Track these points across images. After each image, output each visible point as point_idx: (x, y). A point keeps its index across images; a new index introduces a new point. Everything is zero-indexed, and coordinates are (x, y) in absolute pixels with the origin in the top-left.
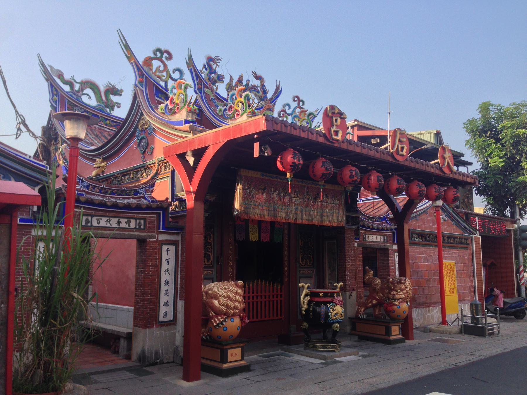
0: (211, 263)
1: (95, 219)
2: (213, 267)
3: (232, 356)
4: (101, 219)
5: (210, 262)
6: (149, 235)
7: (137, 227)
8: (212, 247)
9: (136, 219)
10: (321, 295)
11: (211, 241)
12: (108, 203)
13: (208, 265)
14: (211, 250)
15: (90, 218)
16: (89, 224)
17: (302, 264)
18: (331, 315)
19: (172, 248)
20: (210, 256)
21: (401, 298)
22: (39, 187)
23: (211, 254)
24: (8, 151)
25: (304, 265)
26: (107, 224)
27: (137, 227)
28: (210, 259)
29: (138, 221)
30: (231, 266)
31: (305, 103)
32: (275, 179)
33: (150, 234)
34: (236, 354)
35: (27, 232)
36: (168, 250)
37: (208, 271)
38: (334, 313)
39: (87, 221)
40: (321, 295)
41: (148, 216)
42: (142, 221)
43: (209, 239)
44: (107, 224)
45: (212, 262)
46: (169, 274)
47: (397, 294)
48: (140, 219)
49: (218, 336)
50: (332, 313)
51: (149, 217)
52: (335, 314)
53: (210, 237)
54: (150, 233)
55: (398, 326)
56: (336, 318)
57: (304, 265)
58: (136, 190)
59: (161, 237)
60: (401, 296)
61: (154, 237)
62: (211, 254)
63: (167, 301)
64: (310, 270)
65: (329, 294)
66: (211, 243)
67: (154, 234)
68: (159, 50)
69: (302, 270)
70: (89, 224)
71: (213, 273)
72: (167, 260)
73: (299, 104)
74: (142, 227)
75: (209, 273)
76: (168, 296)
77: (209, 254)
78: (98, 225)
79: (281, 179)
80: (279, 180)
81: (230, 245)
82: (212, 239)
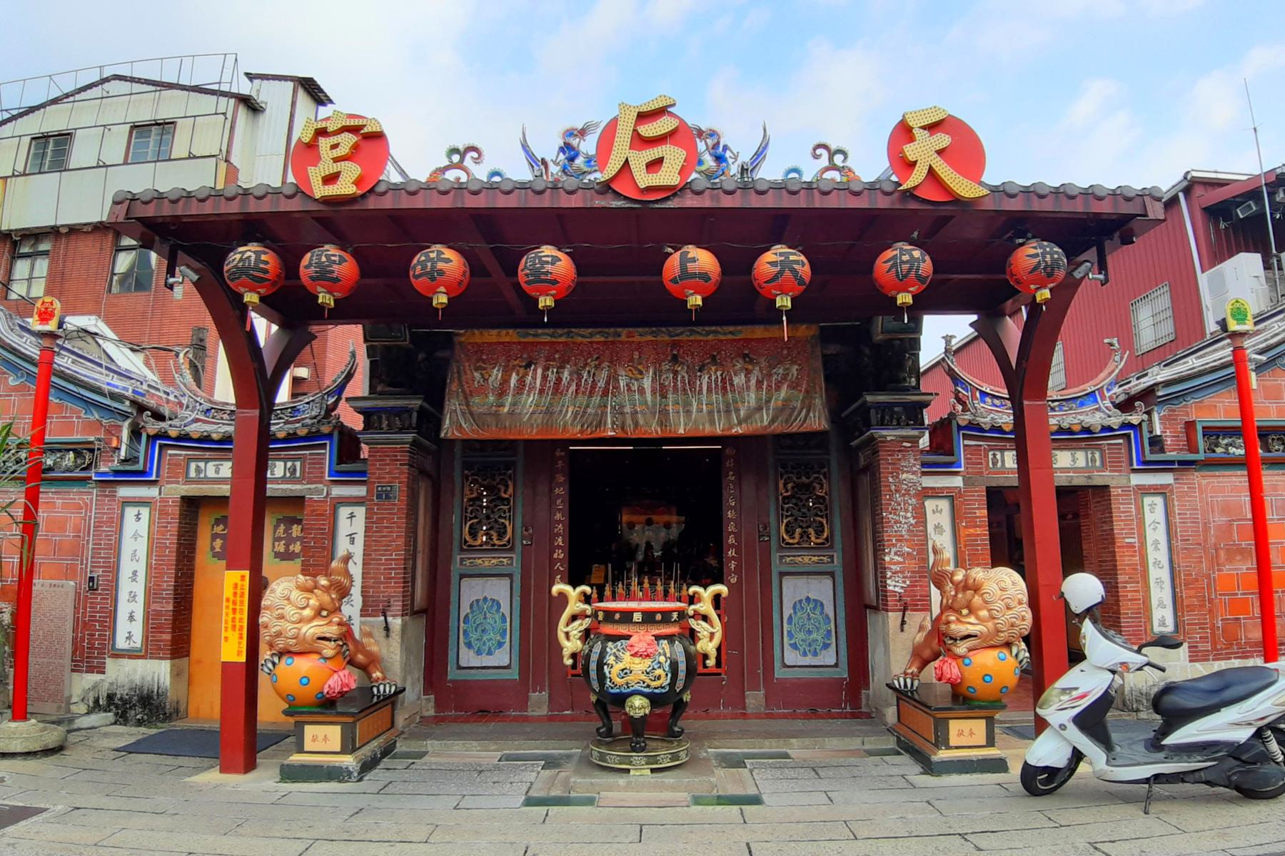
0: (509, 541)
1: (211, 465)
2: (512, 549)
3: (314, 739)
4: (221, 465)
5: (506, 539)
6: (310, 489)
7: (288, 475)
9: (285, 460)
11: (507, 496)
12: (215, 436)
14: (507, 514)
15: (202, 464)
17: (791, 541)
18: (610, 673)
19: (360, 512)
20: (505, 527)
22: (129, 421)
24: (85, 376)
25: (797, 543)
28: (505, 532)
29: (289, 464)
30: (732, 546)
31: (850, 156)
35: (112, 492)
36: (352, 516)
37: (499, 558)
39: (198, 470)
41: (308, 452)
42: (298, 464)
43: (503, 490)
45: (509, 539)
46: (355, 564)
48: (294, 459)
49: (288, 695)
50: (612, 667)
52: (623, 670)
53: (507, 487)
54: (312, 484)
55: (463, 664)
56: (627, 683)
57: (797, 543)
58: (295, 407)
59: (338, 491)
61: (319, 492)
62: (825, 522)
63: (350, 617)
64: (819, 556)
65: (617, 616)
66: (508, 500)
67: (320, 486)
68: (454, 151)
69: (470, 559)
70: (202, 475)
71: (512, 564)
72: (351, 535)
73: (831, 159)
74: (298, 474)
76: (352, 605)
82: (511, 490)
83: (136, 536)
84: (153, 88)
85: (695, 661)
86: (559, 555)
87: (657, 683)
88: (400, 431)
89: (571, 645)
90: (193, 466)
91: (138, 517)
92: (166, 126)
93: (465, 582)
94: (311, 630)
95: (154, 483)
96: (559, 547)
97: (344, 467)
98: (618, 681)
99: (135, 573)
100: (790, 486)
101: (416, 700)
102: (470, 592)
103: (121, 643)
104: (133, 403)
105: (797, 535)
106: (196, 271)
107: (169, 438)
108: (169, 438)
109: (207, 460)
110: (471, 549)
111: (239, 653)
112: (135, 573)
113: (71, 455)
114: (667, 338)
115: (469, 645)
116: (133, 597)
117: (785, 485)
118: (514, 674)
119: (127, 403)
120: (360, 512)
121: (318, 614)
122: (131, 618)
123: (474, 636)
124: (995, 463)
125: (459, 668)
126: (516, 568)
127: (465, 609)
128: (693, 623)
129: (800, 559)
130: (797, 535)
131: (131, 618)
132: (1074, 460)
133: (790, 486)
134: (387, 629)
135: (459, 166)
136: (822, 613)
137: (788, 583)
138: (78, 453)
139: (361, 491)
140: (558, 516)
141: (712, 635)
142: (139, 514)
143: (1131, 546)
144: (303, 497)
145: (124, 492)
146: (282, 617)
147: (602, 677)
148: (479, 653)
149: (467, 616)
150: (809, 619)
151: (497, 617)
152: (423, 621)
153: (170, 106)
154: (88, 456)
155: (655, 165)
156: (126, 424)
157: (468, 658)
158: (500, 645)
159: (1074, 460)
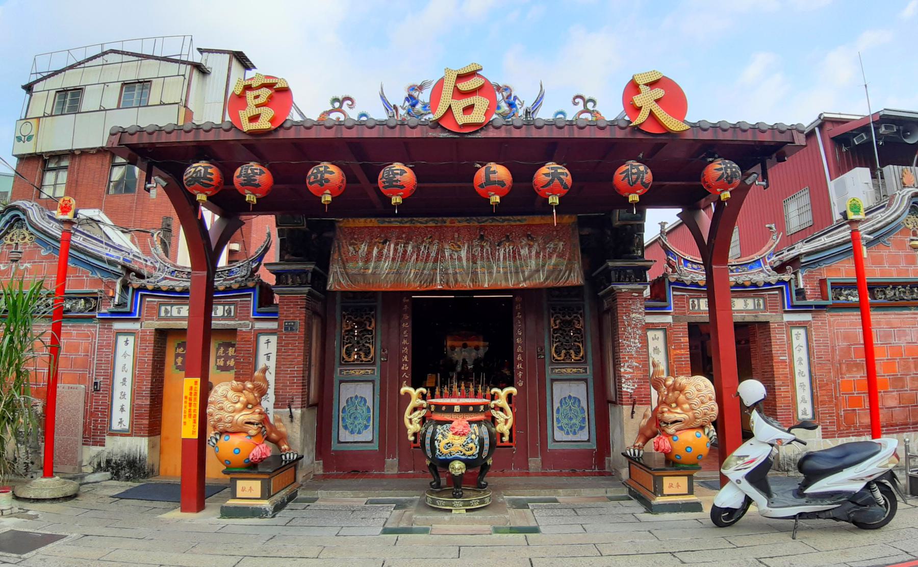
0: (372, 359)
1: (175, 308)
2: (374, 364)
5: (370, 357)
7: (226, 314)
8: (372, 337)
9: (224, 304)
10: (457, 409)
11: (370, 329)
12: (177, 289)
13: (366, 361)
15: (169, 308)
16: (169, 315)
17: (559, 358)
18: (439, 445)
19: (274, 339)
20: (370, 349)
21: (676, 421)
23: (371, 346)
24: (92, 249)
26: (655, 335)
27: (226, 314)
28: (369, 353)
29: (227, 307)
32: (408, 225)
33: (242, 322)
34: (678, 486)
36: (268, 342)
38: (444, 442)
39: (166, 311)
40: (457, 409)
41: (239, 299)
42: (232, 307)
44: (655, 335)
47: (669, 411)
48: (230, 304)
51: (241, 301)
52: (447, 444)
53: (371, 323)
54: (241, 320)
55: (342, 439)
56: (450, 453)
57: (563, 360)
59: (259, 325)
60: (678, 416)
63: (267, 409)
64: (577, 368)
65: (444, 408)
67: (247, 322)
70: (169, 315)
71: (374, 374)
72: (267, 354)
74: (232, 314)
75: (368, 372)
76: (268, 401)
77: (368, 347)
78: (178, 315)
79: (421, 223)
80: (419, 225)
81: (405, 332)
82: (373, 325)
83: (125, 355)
84: (137, 58)
85: (495, 438)
86: (405, 367)
87: (470, 453)
88: (300, 285)
89: (413, 426)
90: (163, 308)
91: (127, 343)
92: (145, 84)
93: (343, 385)
94: (241, 417)
95: (137, 320)
96: (405, 362)
97: (263, 309)
98: (444, 451)
99: (124, 380)
100: (558, 322)
101: (310, 464)
102: (347, 392)
103: (115, 426)
104: (124, 267)
105: (563, 354)
106: (165, 180)
107: (147, 290)
108: (147, 290)
109: (172, 305)
110: (347, 363)
111: (194, 432)
112: (124, 380)
113: (82, 301)
114: (476, 224)
115: (346, 427)
116: (123, 395)
117: (555, 321)
118: (375, 447)
119: (120, 267)
120: (274, 339)
121: (246, 406)
122: (122, 409)
123: (349, 421)
124: (693, 307)
125: (339, 442)
126: (377, 376)
127: (343, 404)
128: (494, 413)
129: (564, 370)
130: (563, 354)
131: (122, 409)
132: (746, 305)
133: (558, 322)
134: (291, 416)
135: (339, 110)
136: (579, 406)
137: (557, 386)
138: (87, 300)
139: (274, 325)
140: (405, 342)
141: (506, 420)
142: (127, 340)
143: (784, 361)
144: (236, 329)
145: (117, 326)
146: (222, 409)
147: (433, 448)
148: (352, 432)
149: (344, 408)
150: (571, 410)
151: (364, 409)
152: (315, 411)
153: (148, 70)
154: (93, 302)
155: (468, 109)
156: (119, 281)
157: (345, 436)
158: (366, 427)
159: (746, 305)
